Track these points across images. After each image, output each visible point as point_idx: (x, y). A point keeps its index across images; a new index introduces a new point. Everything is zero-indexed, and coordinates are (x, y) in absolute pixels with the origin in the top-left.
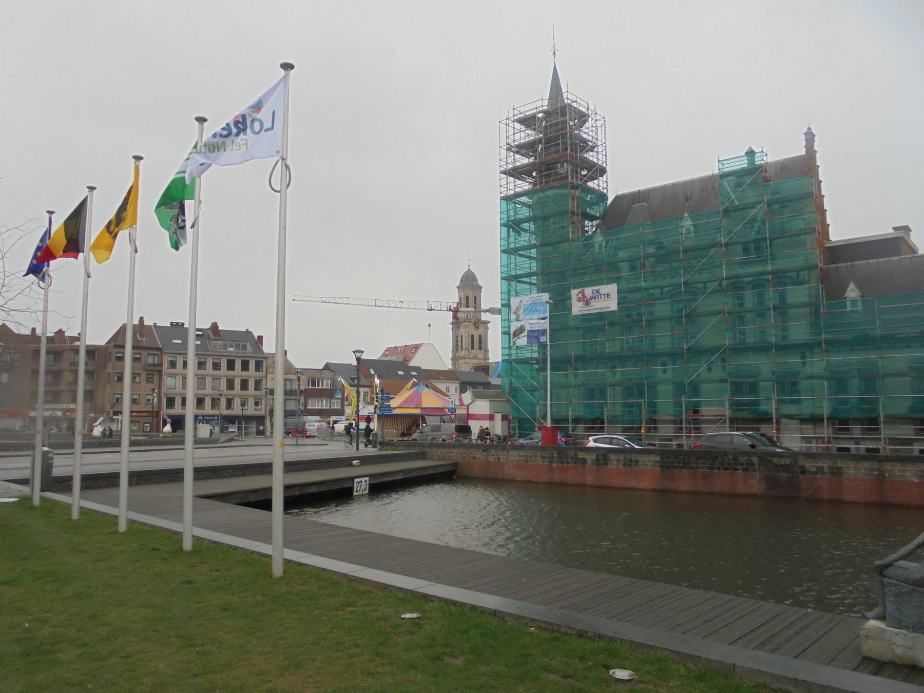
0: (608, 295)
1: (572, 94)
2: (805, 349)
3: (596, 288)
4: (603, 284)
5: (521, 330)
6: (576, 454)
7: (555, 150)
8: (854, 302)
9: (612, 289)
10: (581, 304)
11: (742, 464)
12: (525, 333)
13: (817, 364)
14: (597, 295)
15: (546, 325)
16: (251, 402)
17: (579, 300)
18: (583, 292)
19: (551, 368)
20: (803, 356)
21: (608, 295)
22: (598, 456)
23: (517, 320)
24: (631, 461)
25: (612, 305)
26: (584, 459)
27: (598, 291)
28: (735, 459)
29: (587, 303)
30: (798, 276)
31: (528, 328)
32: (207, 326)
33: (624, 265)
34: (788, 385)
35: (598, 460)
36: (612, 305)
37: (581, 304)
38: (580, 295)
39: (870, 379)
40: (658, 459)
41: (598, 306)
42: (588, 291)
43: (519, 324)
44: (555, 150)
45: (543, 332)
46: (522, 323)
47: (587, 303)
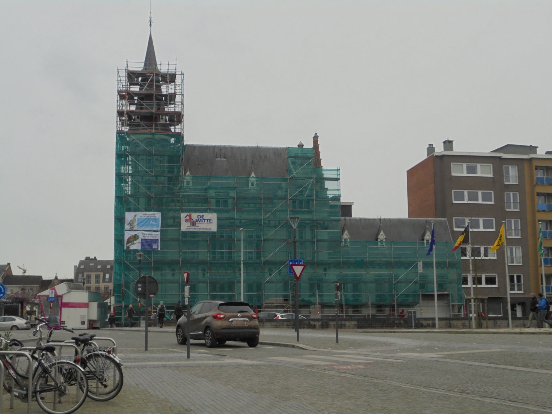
0: (210, 221)
1: (164, 66)
2: (326, 266)
3: (201, 214)
4: (207, 212)
5: (136, 237)
6: (309, 323)
7: (148, 103)
8: (382, 241)
9: (213, 216)
10: (189, 224)
11: (396, 324)
12: (139, 240)
13: (333, 274)
14: (201, 219)
15: (157, 236)
16: (93, 279)
17: (187, 221)
18: (190, 216)
19: (433, 263)
20: (325, 269)
21: (210, 221)
22: (322, 323)
23: (131, 230)
24: (341, 325)
25: (213, 227)
26: (314, 325)
27: (202, 217)
28: (394, 322)
29: (193, 224)
30: (324, 223)
31: (141, 237)
32: (344, 200)
33: (213, 201)
34: (316, 284)
35: (322, 325)
36: (213, 227)
37: (189, 224)
38: (188, 218)
39: (357, 284)
40: (356, 323)
41: (202, 227)
42: (195, 216)
43: (133, 233)
44: (148, 103)
45: (156, 241)
46: (136, 233)
47: (193, 224)
